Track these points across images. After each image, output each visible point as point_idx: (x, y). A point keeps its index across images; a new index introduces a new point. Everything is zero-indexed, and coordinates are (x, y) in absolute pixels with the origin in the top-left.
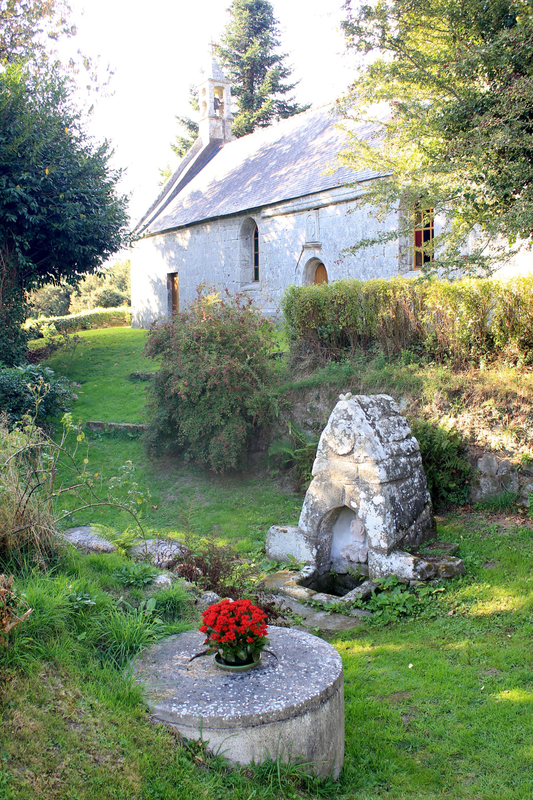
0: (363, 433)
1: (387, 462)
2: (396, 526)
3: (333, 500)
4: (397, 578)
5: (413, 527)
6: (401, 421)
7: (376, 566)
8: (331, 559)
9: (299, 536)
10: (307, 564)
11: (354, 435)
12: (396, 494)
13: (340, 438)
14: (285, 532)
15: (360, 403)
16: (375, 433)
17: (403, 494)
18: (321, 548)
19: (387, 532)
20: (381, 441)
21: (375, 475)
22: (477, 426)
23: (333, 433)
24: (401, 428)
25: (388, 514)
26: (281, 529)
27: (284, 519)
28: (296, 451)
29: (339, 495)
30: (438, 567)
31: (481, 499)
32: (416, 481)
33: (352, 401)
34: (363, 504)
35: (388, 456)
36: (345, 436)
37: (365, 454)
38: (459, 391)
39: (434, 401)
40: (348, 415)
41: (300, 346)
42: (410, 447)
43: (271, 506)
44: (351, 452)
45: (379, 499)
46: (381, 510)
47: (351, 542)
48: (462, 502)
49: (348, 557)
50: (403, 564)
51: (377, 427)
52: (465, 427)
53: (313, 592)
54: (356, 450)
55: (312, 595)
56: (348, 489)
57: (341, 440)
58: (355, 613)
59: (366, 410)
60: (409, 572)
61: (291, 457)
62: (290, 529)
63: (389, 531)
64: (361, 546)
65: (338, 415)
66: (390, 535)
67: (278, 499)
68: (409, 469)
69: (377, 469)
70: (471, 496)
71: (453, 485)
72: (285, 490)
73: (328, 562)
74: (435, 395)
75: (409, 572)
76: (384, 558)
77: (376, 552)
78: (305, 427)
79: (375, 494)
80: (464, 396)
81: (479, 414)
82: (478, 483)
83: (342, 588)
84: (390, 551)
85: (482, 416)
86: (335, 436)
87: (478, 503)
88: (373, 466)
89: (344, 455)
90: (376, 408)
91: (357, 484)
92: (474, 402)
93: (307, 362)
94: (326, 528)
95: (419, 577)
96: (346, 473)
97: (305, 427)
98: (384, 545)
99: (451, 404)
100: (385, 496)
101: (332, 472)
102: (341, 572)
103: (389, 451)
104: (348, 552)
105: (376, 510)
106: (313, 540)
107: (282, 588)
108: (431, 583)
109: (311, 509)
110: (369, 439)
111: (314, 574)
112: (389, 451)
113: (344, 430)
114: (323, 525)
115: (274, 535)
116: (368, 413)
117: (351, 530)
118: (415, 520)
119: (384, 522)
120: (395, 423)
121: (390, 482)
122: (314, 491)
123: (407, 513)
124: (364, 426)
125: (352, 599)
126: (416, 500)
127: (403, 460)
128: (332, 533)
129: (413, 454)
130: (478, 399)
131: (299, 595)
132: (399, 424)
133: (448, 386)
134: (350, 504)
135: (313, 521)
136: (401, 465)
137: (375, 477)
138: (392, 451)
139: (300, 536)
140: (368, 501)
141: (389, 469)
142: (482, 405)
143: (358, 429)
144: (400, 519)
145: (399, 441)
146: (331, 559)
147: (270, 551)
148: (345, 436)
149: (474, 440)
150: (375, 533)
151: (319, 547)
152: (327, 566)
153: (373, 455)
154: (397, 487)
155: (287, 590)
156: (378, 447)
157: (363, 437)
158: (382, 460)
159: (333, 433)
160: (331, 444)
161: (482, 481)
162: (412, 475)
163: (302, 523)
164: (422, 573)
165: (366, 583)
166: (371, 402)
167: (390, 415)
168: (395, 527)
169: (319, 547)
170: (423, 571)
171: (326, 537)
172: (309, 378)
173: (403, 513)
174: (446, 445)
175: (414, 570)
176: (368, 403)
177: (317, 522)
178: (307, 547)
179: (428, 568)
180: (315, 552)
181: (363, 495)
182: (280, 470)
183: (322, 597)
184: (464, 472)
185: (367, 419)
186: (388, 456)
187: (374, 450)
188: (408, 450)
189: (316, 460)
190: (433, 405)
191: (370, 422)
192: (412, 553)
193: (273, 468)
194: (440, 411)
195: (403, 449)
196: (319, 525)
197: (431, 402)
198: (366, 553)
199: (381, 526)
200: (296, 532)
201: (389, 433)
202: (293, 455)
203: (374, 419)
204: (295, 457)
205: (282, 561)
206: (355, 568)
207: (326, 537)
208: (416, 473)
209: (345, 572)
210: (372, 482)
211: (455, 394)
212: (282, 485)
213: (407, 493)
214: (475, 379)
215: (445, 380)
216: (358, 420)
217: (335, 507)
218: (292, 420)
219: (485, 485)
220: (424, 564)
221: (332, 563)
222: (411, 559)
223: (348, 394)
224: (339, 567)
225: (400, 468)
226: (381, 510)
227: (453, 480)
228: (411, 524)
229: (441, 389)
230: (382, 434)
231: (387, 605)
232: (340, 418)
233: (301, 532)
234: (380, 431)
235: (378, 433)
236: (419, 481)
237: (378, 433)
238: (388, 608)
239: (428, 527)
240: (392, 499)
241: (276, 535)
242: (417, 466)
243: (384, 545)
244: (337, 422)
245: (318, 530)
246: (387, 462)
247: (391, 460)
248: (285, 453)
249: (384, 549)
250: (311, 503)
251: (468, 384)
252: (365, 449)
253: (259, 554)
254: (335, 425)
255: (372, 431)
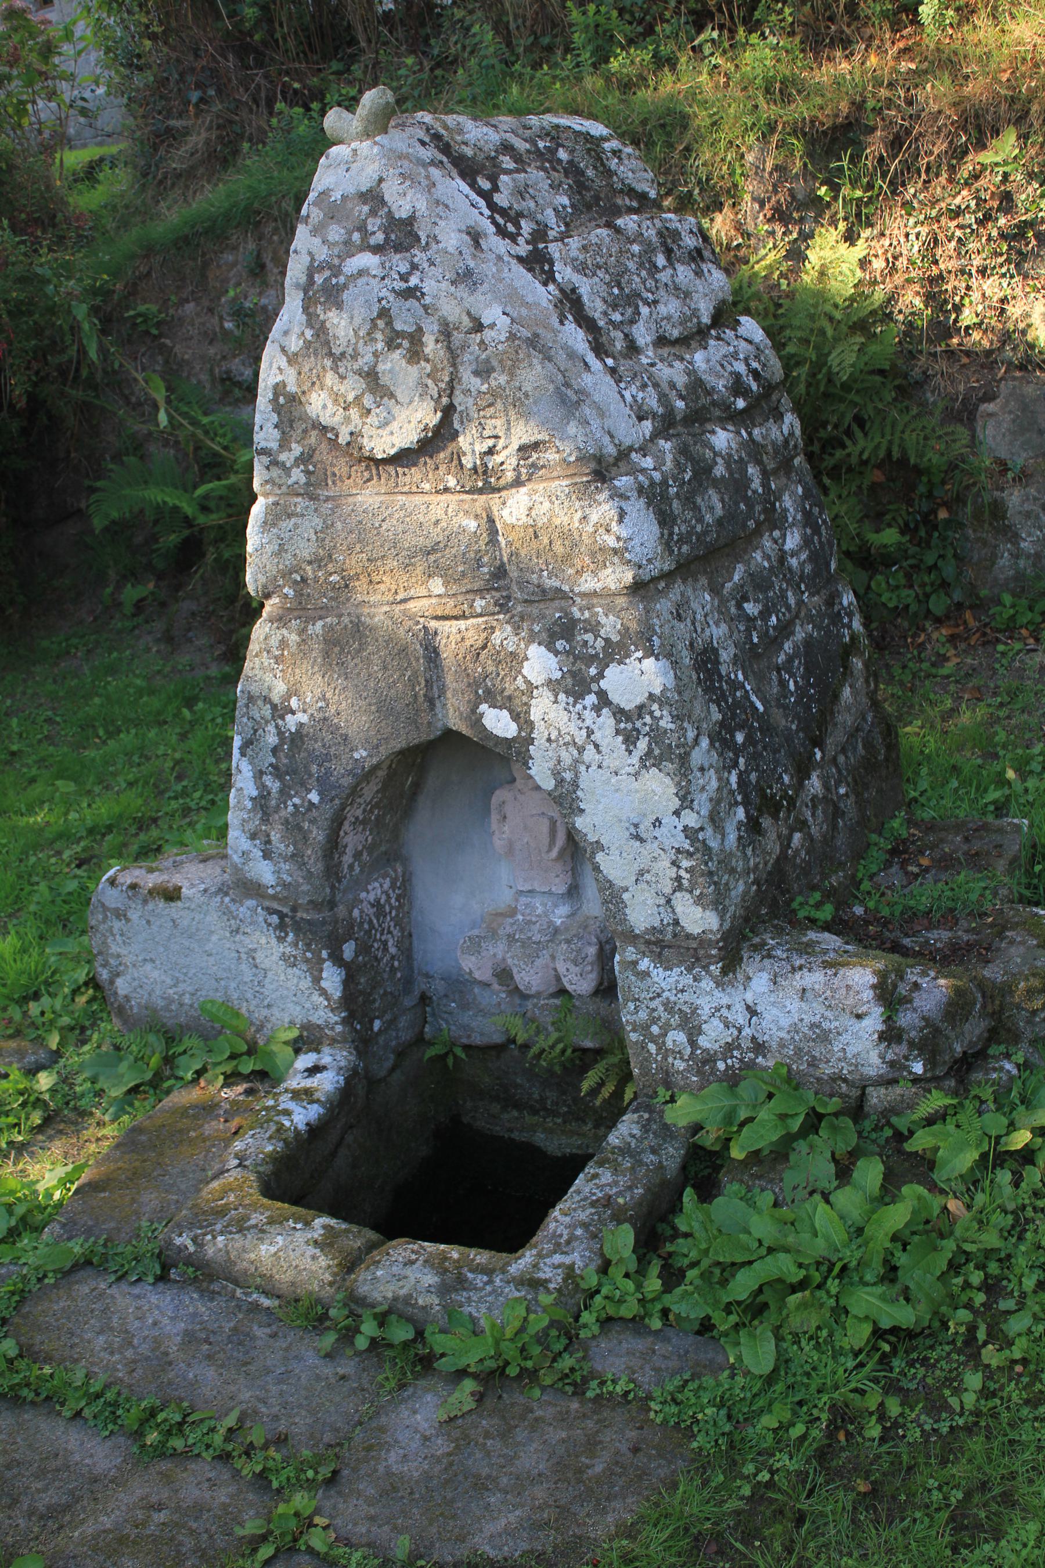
0: (492, 314)
1: (648, 462)
2: (746, 803)
3: (384, 709)
4: (793, 1081)
5: (815, 784)
6: (676, 235)
7: (666, 1029)
8: (421, 985)
9: (243, 911)
10: (306, 1040)
11: (446, 332)
12: (718, 632)
13: (366, 359)
14: (172, 895)
15: (446, 149)
16: (558, 305)
17: (750, 619)
18: (364, 948)
19: (707, 849)
20: (599, 349)
21: (592, 536)
22: (953, 265)
23: (321, 339)
24: (684, 273)
25: (702, 753)
26: (151, 880)
27: (184, 793)
28: (200, 491)
29: (412, 682)
30: (1006, 989)
31: (1019, 576)
32: (792, 541)
33: (398, 139)
34: (548, 712)
35: (647, 426)
36: (391, 345)
37: (523, 433)
38: (848, 126)
39: (750, 188)
40: (393, 224)
41: (163, 82)
42: (740, 367)
43: (127, 738)
44: (437, 440)
45: (639, 678)
46: (656, 735)
47: (505, 898)
48: (938, 604)
49: (504, 975)
50: (821, 1008)
51: (564, 273)
52: (899, 279)
53: (357, 1237)
54: (465, 419)
55: (350, 1265)
56: (455, 636)
57: (371, 377)
58: (617, 1362)
59: (485, 185)
60: (860, 1045)
61: (188, 522)
62: (193, 877)
63: (714, 844)
64: (560, 915)
65: (336, 233)
66: (725, 860)
67: (156, 703)
68: (756, 484)
69: (604, 510)
70: (970, 573)
71: (890, 537)
72: (184, 659)
73: (408, 1002)
74: (750, 158)
75: (860, 1045)
76: (707, 984)
77: (659, 958)
78: (227, 393)
79: (615, 652)
80: (875, 146)
81: (956, 213)
82: (998, 510)
83: (495, 1108)
84: (730, 953)
85: (970, 219)
86: (338, 359)
87: (1007, 599)
88: (583, 492)
89: (404, 458)
90: (535, 175)
91: (503, 606)
92: (923, 162)
93: (197, 140)
94: (371, 849)
95: (918, 1068)
96: (431, 556)
97: (227, 393)
98: (698, 919)
99: (823, 191)
100: (668, 654)
101: (354, 563)
102: (477, 1040)
103: (652, 402)
104: (498, 950)
105: (630, 740)
106: (317, 923)
107: (183, 1240)
108: (984, 1083)
109: (277, 772)
110: (533, 342)
111: (345, 1094)
112: (652, 402)
113: (384, 313)
114: (352, 839)
115: (120, 914)
116: (502, 199)
117: (499, 843)
118: (818, 742)
119: (686, 800)
120: (649, 250)
121: (683, 570)
122: (280, 671)
123: (780, 720)
124: (489, 268)
125: (575, 1258)
126: (808, 642)
127: (722, 439)
128: (405, 861)
129: (762, 405)
130: (940, 147)
131: (284, 1278)
132: (669, 252)
133: (801, 110)
134: (476, 721)
135: (293, 828)
136: (720, 470)
137: (600, 556)
138: (663, 398)
139: (247, 908)
140: (579, 696)
141: (665, 498)
142: (964, 173)
143: (462, 291)
144: (754, 758)
145: (683, 341)
146: (421, 985)
147: (122, 986)
148: (391, 345)
149: (943, 329)
150: (643, 862)
151: (348, 950)
152: (403, 1022)
153: (572, 429)
154: (715, 590)
155: (218, 1245)
156: (587, 379)
157: (498, 333)
158: (624, 454)
159: (321, 339)
160: (319, 405)
161: (1014, 498)
162: (774, 520)
163: (245, 844)
164: (929, 1045)
165: (627, 1129)
166: (507, 148)
167: (618, 212)
168: (741, 813)
169: (348, 950)
170: (937, 1031)
171: (376, 890)
172: (211, 197)
173: (767, 728)
174: (851, 358)
175: (890, 1035)
176: (490, 148)
177: (318, 835)
178: (290, 961)
179: (957, 1008)
180: (332, 979)
181: (539, 664)
182: (160, 577)
183: (407, 1271)
184: (927, 471)
185: (501, 232)
186: (647, 426)
187: (570, 401)
188: (738, 387)
189: (257, 510)
190: (748, 204)
191: (523, 249)
192: (863, 934)
193: (131, 575)
194: (779, 230)
195: (710, 380)
196: (333, 845)
197: (734, 192)
198: (592, 951)
199: (669, 820)
200: (222, 890)
201: (632, 299)
202: (189, 510)
203: (540, 234)
204: (202, 519)
205: (185, 1029)
206: (547, 1019)
207: (376, 890)
208: (788, 502)
209: (498, 1039)
210: (588, 583)
211: (833, 142)
212: (168, 638)
213: (765, 615)
214: (905, 66)
215: (781, 90)
216: (451, 239)
217: (399, 744)
218: (173, 374)
219: (1028, 515)
220: (933, 990)
221: (424, 999)
222: (861, 977)
223: (370, 98)
224: (466, 1018)
225: (716, 483)
226: (656, 735)
227: (877, 518)
228: (802, 772)
229: (771, 127)
230: (595, 307)
231: (794, 1289)
232: (349, 249)
233: (250, 888)
234: (584, 291)
235: (571, 303)
236: (807, 542)
237: (571, 303)
238: (803, 1305)
239: (869, 765)
240: (706, 660)
241: (134, 915)
242: (785, 466)
243: (698, 919)
244: (337, 271)
245: (332, 872)
246: (648, 462)
247: (666, 445)
248: (159, 509)
249: (702, 940)
250: (272, 739)
251: (884, 93)
252: (519, 404)
253: (82, 1000)
254: (324, 292)
255: (543, 295)
